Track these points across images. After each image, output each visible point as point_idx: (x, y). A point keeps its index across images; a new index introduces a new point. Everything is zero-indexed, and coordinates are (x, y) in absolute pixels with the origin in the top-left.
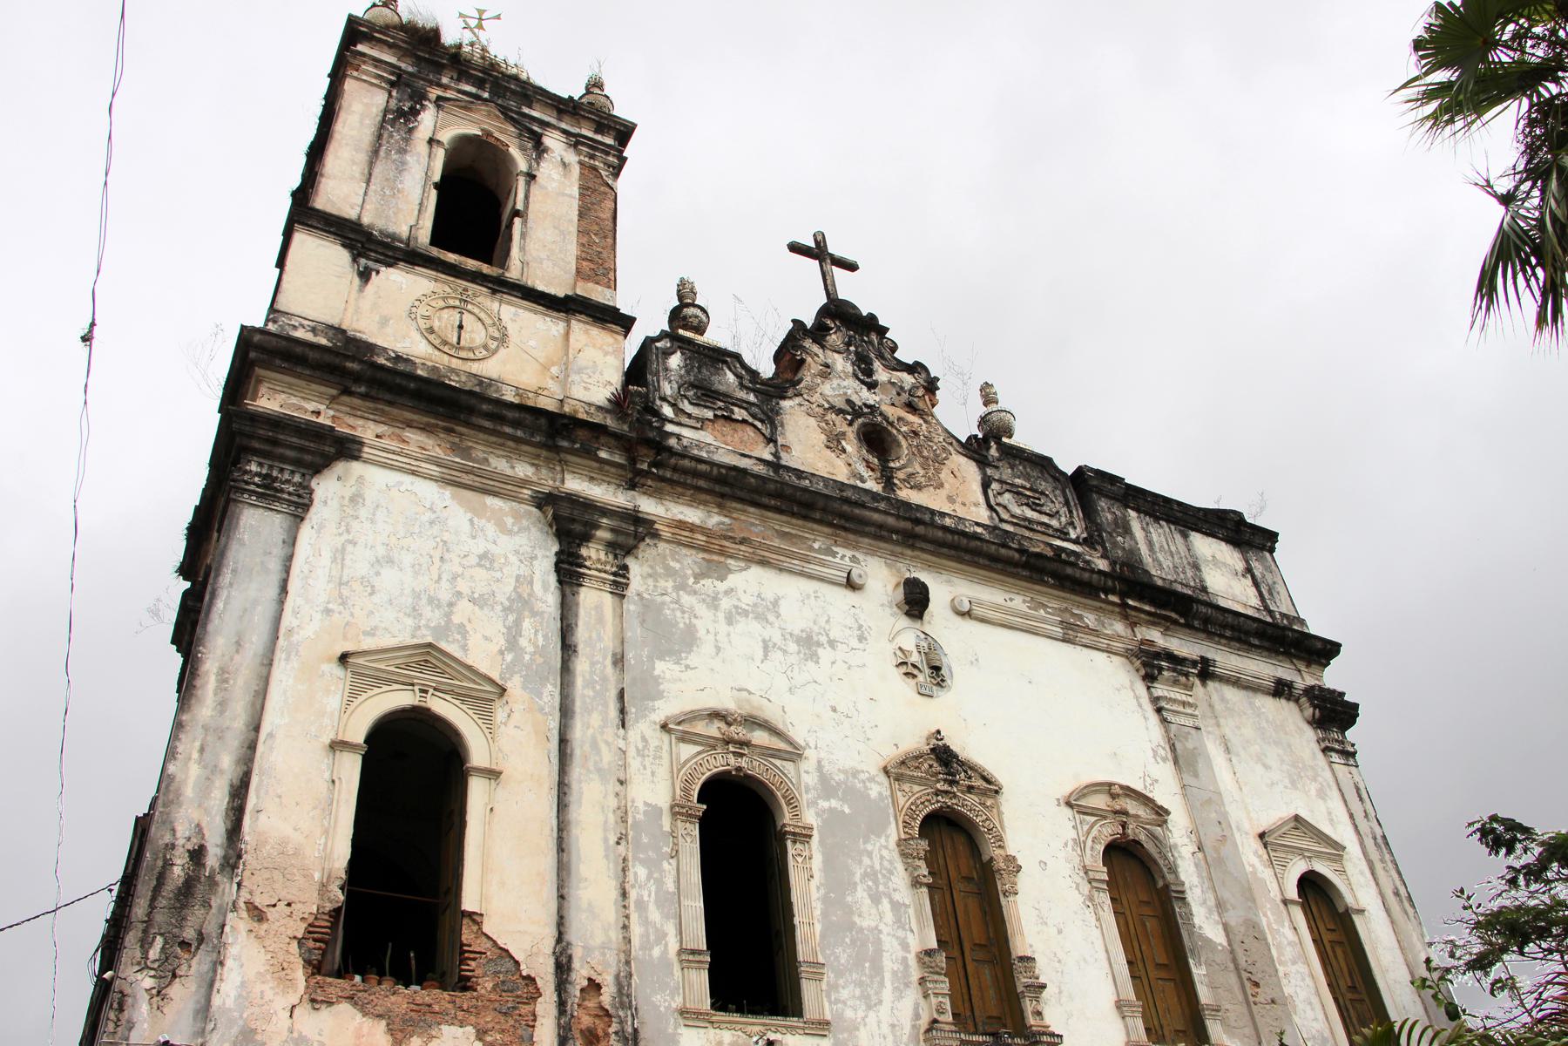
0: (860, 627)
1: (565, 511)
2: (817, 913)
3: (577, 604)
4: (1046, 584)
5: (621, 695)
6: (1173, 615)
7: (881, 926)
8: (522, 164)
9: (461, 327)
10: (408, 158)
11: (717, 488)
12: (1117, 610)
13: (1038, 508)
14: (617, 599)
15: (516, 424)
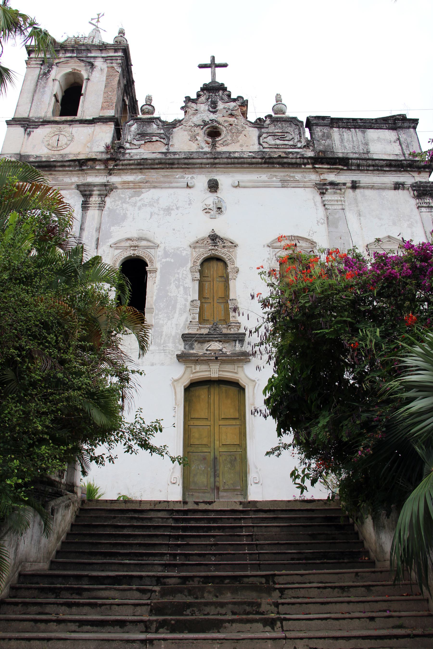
0: (190, 200)
1: (82, 188)
2: (155, 294)
3: (86, 216)
4: (275, 168)
5: (98, 239)
6: (340, 167)
7: (179, 295)
8: (85, 77)
9: (58, 140)
10: (46, 89)
11: (138, 167)
12: (312, 170)
13: (285, 139)
14: (100, 211)
15: (69, 166)
